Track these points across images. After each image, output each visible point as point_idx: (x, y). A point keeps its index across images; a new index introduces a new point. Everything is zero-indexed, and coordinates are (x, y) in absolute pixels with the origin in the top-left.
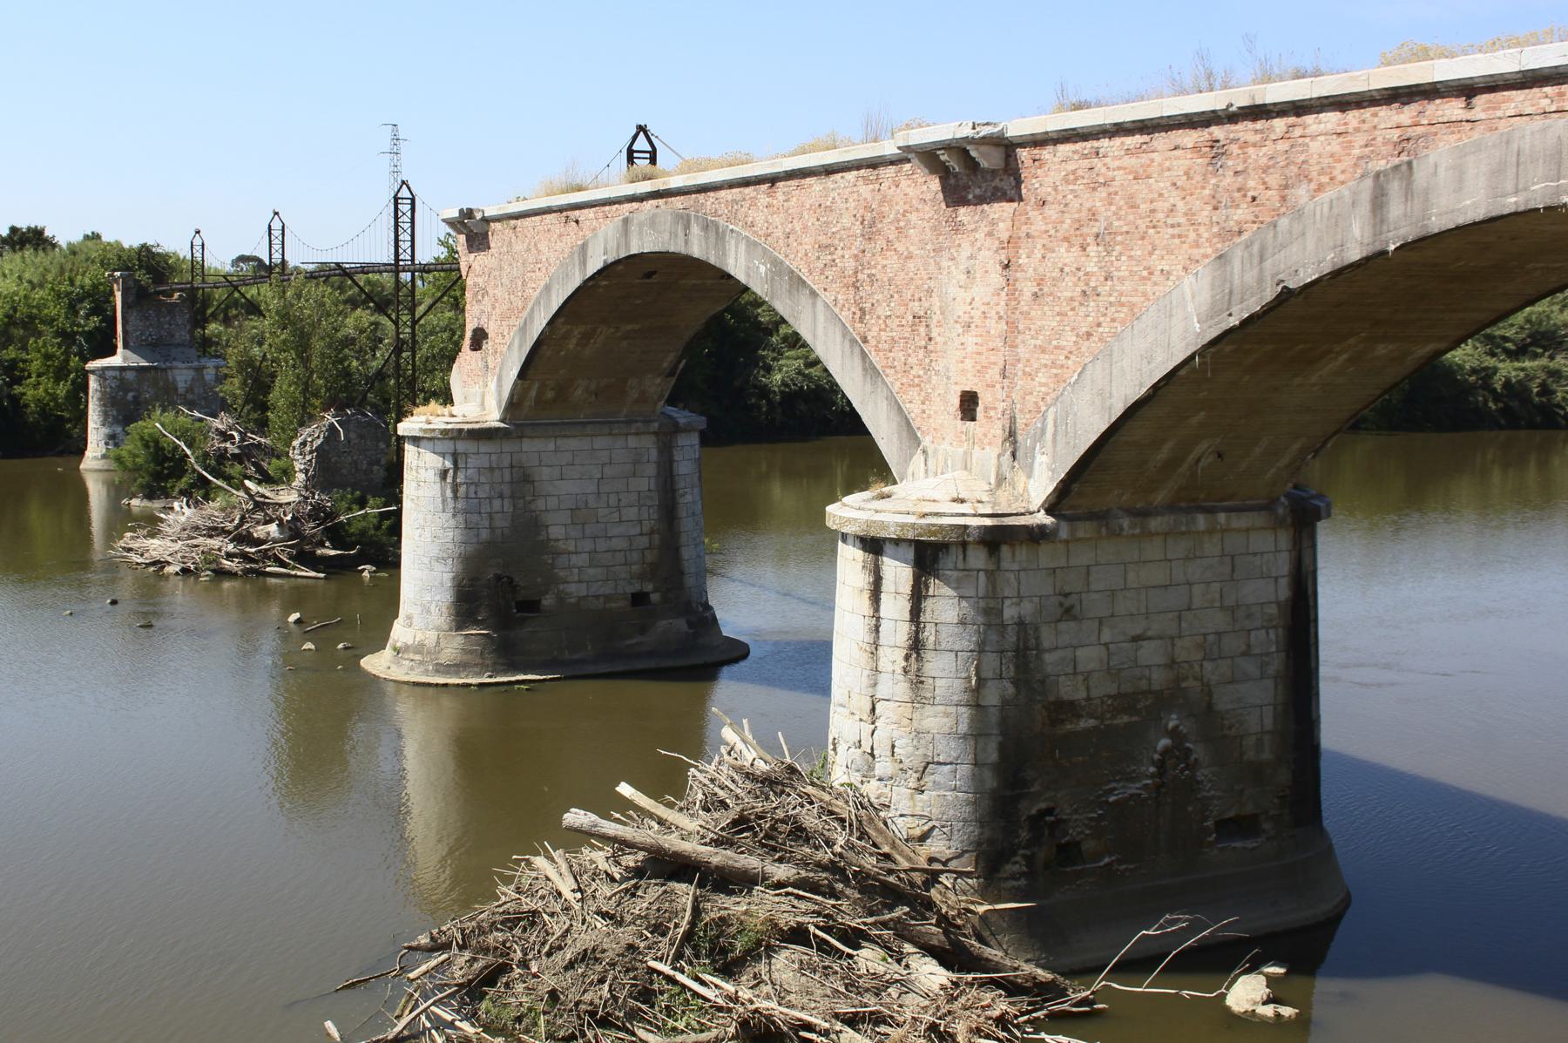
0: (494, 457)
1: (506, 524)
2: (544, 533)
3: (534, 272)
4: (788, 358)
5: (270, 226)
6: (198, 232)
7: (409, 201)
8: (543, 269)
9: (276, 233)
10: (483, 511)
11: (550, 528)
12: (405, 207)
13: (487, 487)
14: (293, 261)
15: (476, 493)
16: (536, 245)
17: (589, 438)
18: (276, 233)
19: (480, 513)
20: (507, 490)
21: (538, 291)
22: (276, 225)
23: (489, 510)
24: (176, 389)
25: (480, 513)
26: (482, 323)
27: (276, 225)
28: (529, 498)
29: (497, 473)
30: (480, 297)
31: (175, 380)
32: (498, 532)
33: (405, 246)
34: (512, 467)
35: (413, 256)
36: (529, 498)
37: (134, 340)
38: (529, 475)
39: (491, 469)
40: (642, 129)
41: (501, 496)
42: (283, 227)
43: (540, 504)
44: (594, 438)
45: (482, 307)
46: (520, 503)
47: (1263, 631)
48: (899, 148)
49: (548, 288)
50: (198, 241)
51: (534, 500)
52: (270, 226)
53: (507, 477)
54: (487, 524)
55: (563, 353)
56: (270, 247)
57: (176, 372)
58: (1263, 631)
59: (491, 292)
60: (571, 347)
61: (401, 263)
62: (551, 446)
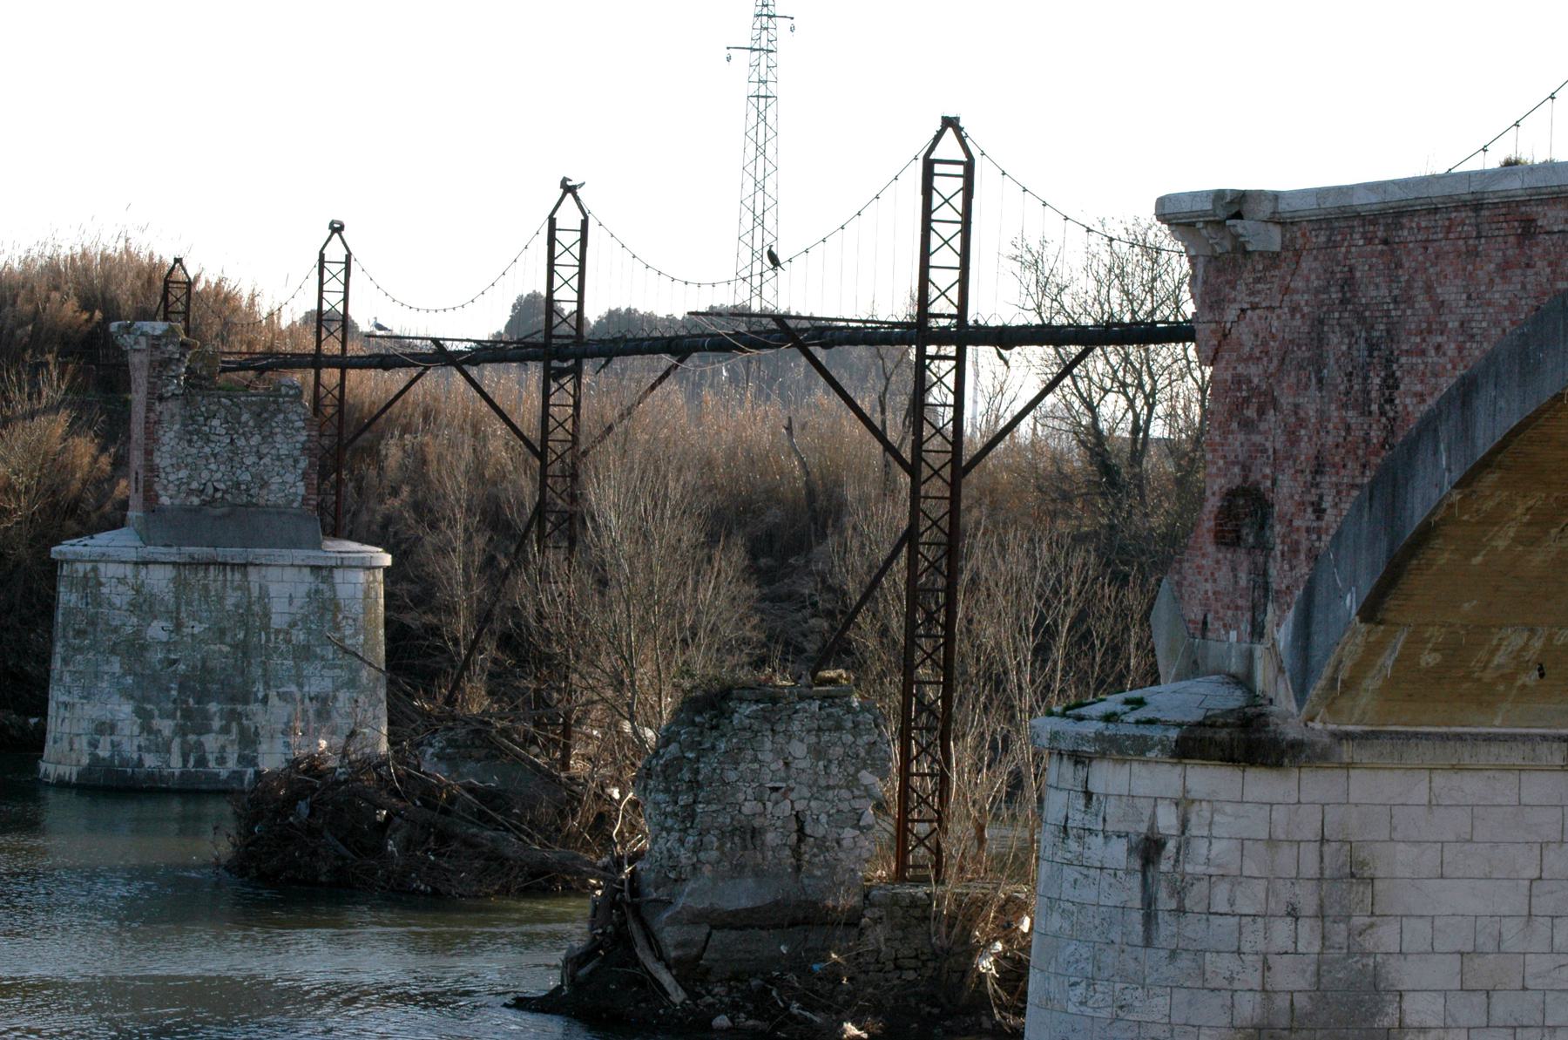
0: (1279, 814)
1: (1303, 985)
2: (1392, 1009)
3: (1423, 353)
4: (512, 514)
5: (322, 256)
6: (337, 228)
7: (960, 170)
8: (1451, 350)
9: (568, 238)
10: (1246, 948)
11: (1408, 998)
12: (948, 185)
13: (1259, 888)
14: (362, 319)
15: (1232, 903)
16: (1429, 289)
17: (1511, 777)
18: (568, 238)
19: (1239, 952)
20: (1307, 901)
21: (1431, 401)
22: (569, 217)
23: (1261, 947)
24: (267, 615)
25: (1239, 952)
26: (1255, 476)
27: (569, 217)
28: (1359, 921)
29: (1286, 856)
30: (1251, 413)
31: (264, 594)
32: (1282, 1002)
33: (943, 279)
34: (1323, 840)
35: (963, 305)
36: (1359, 921)
37: (172, 489)
38: (1363, 864)
39: (1272, 842)
40: (950, 123)
41: (1293, 913)
42: (585, 223)
43: (1386, 937)
44: (1524, 776)
45: (1257, 438)
46: (1339, 933)
47: (1246, 873)
48: (253, 297)
49: (1467, 389)
50: (335, 252)
51: (1372, 925)
52: (322, 256)
53: (1310, 867)
54: (1254, 980)
55: (1477, 560)
56: (346, 285)
57: (273, 573)
58: (1246, 873)
59: (1286, 401)
60: (1501, 544)
61: (554, 341)
62: (1420, 793)
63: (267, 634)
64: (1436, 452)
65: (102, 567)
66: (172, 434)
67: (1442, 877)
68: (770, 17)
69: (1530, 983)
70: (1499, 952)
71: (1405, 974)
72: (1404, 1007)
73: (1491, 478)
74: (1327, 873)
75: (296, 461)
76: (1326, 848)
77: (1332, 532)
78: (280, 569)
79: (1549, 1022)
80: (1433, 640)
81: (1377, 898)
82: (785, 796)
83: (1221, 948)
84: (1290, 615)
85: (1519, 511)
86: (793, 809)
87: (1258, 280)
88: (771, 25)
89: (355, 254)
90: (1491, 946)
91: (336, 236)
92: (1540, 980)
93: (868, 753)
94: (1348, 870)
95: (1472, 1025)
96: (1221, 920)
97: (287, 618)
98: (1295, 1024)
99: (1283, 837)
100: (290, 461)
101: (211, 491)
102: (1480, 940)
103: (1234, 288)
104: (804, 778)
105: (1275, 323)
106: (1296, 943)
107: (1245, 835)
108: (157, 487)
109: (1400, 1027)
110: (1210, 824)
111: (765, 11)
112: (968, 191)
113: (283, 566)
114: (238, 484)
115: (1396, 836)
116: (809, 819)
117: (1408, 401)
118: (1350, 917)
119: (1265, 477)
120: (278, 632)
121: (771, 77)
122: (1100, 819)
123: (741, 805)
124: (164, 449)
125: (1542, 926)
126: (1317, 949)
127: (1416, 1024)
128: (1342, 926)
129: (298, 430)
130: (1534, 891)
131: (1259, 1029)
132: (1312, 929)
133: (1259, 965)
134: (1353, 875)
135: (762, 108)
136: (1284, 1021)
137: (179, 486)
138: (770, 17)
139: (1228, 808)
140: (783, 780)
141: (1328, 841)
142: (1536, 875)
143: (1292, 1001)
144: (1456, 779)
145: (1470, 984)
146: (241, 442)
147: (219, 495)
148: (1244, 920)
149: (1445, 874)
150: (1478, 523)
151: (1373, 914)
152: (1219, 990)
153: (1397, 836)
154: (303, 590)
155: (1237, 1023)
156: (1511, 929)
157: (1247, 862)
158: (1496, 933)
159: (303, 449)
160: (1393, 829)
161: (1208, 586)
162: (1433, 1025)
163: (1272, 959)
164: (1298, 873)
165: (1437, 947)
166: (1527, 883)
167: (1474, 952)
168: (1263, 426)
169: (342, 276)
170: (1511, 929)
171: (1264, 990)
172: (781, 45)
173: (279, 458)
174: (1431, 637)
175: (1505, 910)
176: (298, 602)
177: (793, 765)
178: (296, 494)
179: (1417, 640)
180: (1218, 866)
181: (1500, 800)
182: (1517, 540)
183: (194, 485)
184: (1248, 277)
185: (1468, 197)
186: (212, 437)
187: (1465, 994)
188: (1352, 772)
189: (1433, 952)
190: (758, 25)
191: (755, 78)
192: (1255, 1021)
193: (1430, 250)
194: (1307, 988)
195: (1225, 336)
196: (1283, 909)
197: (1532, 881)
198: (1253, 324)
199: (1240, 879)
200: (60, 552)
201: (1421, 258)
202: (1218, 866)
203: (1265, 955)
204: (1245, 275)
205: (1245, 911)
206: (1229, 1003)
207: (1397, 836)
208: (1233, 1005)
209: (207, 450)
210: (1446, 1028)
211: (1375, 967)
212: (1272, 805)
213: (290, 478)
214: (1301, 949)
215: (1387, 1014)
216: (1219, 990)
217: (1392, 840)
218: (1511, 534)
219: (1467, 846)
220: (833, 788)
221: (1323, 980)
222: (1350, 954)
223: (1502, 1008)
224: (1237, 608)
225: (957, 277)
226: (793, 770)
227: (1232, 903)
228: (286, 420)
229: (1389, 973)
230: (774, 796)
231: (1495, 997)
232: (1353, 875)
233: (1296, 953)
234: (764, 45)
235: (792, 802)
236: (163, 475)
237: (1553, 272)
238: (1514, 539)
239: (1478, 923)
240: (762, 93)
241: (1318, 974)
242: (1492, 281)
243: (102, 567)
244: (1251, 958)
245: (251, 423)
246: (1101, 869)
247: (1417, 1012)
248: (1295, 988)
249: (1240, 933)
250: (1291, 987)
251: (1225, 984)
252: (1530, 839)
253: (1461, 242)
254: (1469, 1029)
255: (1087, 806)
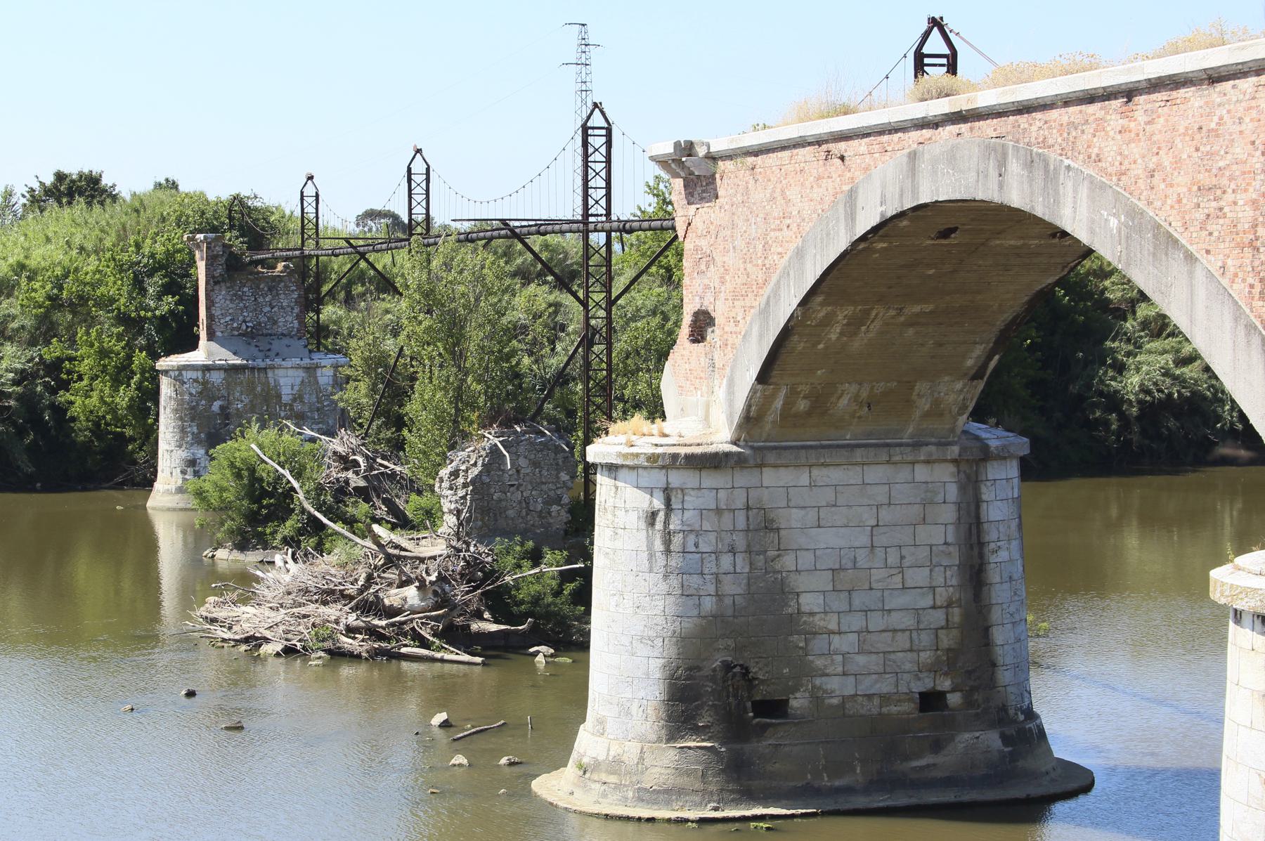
0: (722, 494)
7: (603, 132)
8: (794, 227)
10: (706, 571)
12: (597, 141)
13: (712, 537)
15: (696, 545)
17: (859, 469)
19: (702, 574)
20: (740, 543)
22: (419, 167)
23: (714, 570)
25: (702, 574)
26: (706, 303)
27: (419, 167)
28: (772, 553)
29: (727, 518)
30: (703, 267)
31: (277, 385)
32: (728, 601)
34: (748, 508)
38: (773, 521)
39: (718, 511)
41: (732, 551)
43: (788, 561)
44: (865, 467)
50: (310, 191)
51: (779, 556)
53: (741, 523)
55: (821, 346)
57: (280, 372)
59: (719, 259)
60: (834, 337)
62: (804, 479)
63: (280, 407)
64: (789, 285)
65: (184, 373)
66: (221, 297)
67: (819, 527)
68: (586, 45)
69: (874, 585)
70: (855, 568)
71: (800, 582)
72: (800, 601)
73: (819, 299)
74: (751, 527)
75: (293, 309)
76: (750, 512)
77: (743, 333)
78: (285, 370)
79: (886, 608)
80: (803, 393)
81: (781, 541)
82: (518, 489)
83: (692, 571)
84: (725, 381)
85: (840, 318)
86: (522, 496)
87: (703, 191)
88: (587, 50)
89: (320, 193)
90: (850, 565)
91: (310, 182)
92: (880, 584)
93: (563, 462)
94: (763, 525)
95: (841, 610)
96: (690, 556)
97: (291, 397)
98: (736, 614)
99: (725, 507)
100: (289, 309)
101: (244, 327)
102: (843, 562)
103: (692, 196)
104: (528, 478)
105: (712, 215)
106: (735, 567)
107: (703, 507)
108: (214, 327)
109: (798, 613)
110: (683, 502)
111: (583, 42)
112: (609, 144)
113: (287, 368)
114: (260, 324)
115: (791, 505)
116: (531, 501)
117: (775, 257)
118: (766, 551)
119: (711, 303)
120: (286, 405)
121: (588, 80)
122: (623, 501)
123: (493, 495)
124: (217, 305)
125: (880, 553)
126: (747, 570)
127: (808, 611)
128: (762, 557)
129: (293, 291)
130: (874, 533)
131: (714, 616)
132: (744, 560)
133: (714, 581)
134: (766, 528)
135: (584, 96)
136: (730, 612)
137: (226, 326)
138: (586, 45)
139: (692, 493)
140: (516, 480)
141: (751, 509)
142: (875, 523)
143: (734, 601)
144: (825, 471)
145: (839, 587)
146: (261, 300)
147: (249, 330)
148: (704, 555)
149: (821, 525)
150: (816, 326)
151: (779, 550)
152: (691, 596)
153: (791, 504)
154: (298, 381)
155: (703, 614)
156: (862, 555)
157: (704, 522)
158: (853, 557)
159: (296, 302)
160: (789, 500)
161: (687, 366)
162: (817, 611)
163: (722, 577)
164: (734, 527)
165: (818, 567)
166: (869, 528)
167: (840, 569)
168: (709, 274)
169: (314, 204)
170: (862, 555)
171: (717, 595)
172: (593, 61)
173: (282, 307)
174: (802, 390)
175: (857, 544)
176: (296, 388)
177: (522, 472)
178: (293, 327)
179: (793, 393)
180: (688, 525)
181: (852, 482)
182: (842, 334)
183: (235, 325)
184: (699, 189)
185: (799, 140)
186: (244, 298)
187: (836, 593)
188: (764, 469)
189: (816, 570)
190: (580, 50)
191: (579, 80)
192: (713, 612)
193: (783, 170)
194: (742, 592)
195: (689, 224)
196: (726, 549)
197: (872, 527)
198: (702, 216)
199: (701, 532)
200: (161, 365)
201: (779, 175)
202: (688, 525)
203: (717, 574)
204: (698, 189)
205: (704, 550)
206: (698, 603)
207: (791, 504)
208: (700, 604)
209: (241, 305)
210: (825, 613)
211: (782, 580)
212: (717, 489)
213: (290, 319)
214: (738, 570)
215: (790, 606)
216: (691, 596)
217: (789, 507)
218: (838, 331)
219: (833, 509)
220: (545, 483)
221: (752, 588)
222: (767, 573)
223: (858, 601)
224: (701, 378)
225: (604, 193)
226: (521, 475)
227: (696, 545)
228: (286, 286)
229: (790, 582)
230: (512, 489)
231: (854, 594)
232: (766, 528)
233: (735, 573)
234: (583, 61)
235: (522, 492)
236: (217, 320)
237: (841, 180)
238: (840, 333)
239: (842, 552)
240: (584, 88)
241: (749, 584)
242: (812, 187)
243: (184, 373)
244: (709, 577)
245: (266, 289)
246: (625, 528)
247: (808, 604)
248: (735, 593)
249: (702, 563)
250: (732, 593)
251: (694, 592)
252: (871, 502)
253: (797, 165)
254: (839, 613)
255: (616, 493)
